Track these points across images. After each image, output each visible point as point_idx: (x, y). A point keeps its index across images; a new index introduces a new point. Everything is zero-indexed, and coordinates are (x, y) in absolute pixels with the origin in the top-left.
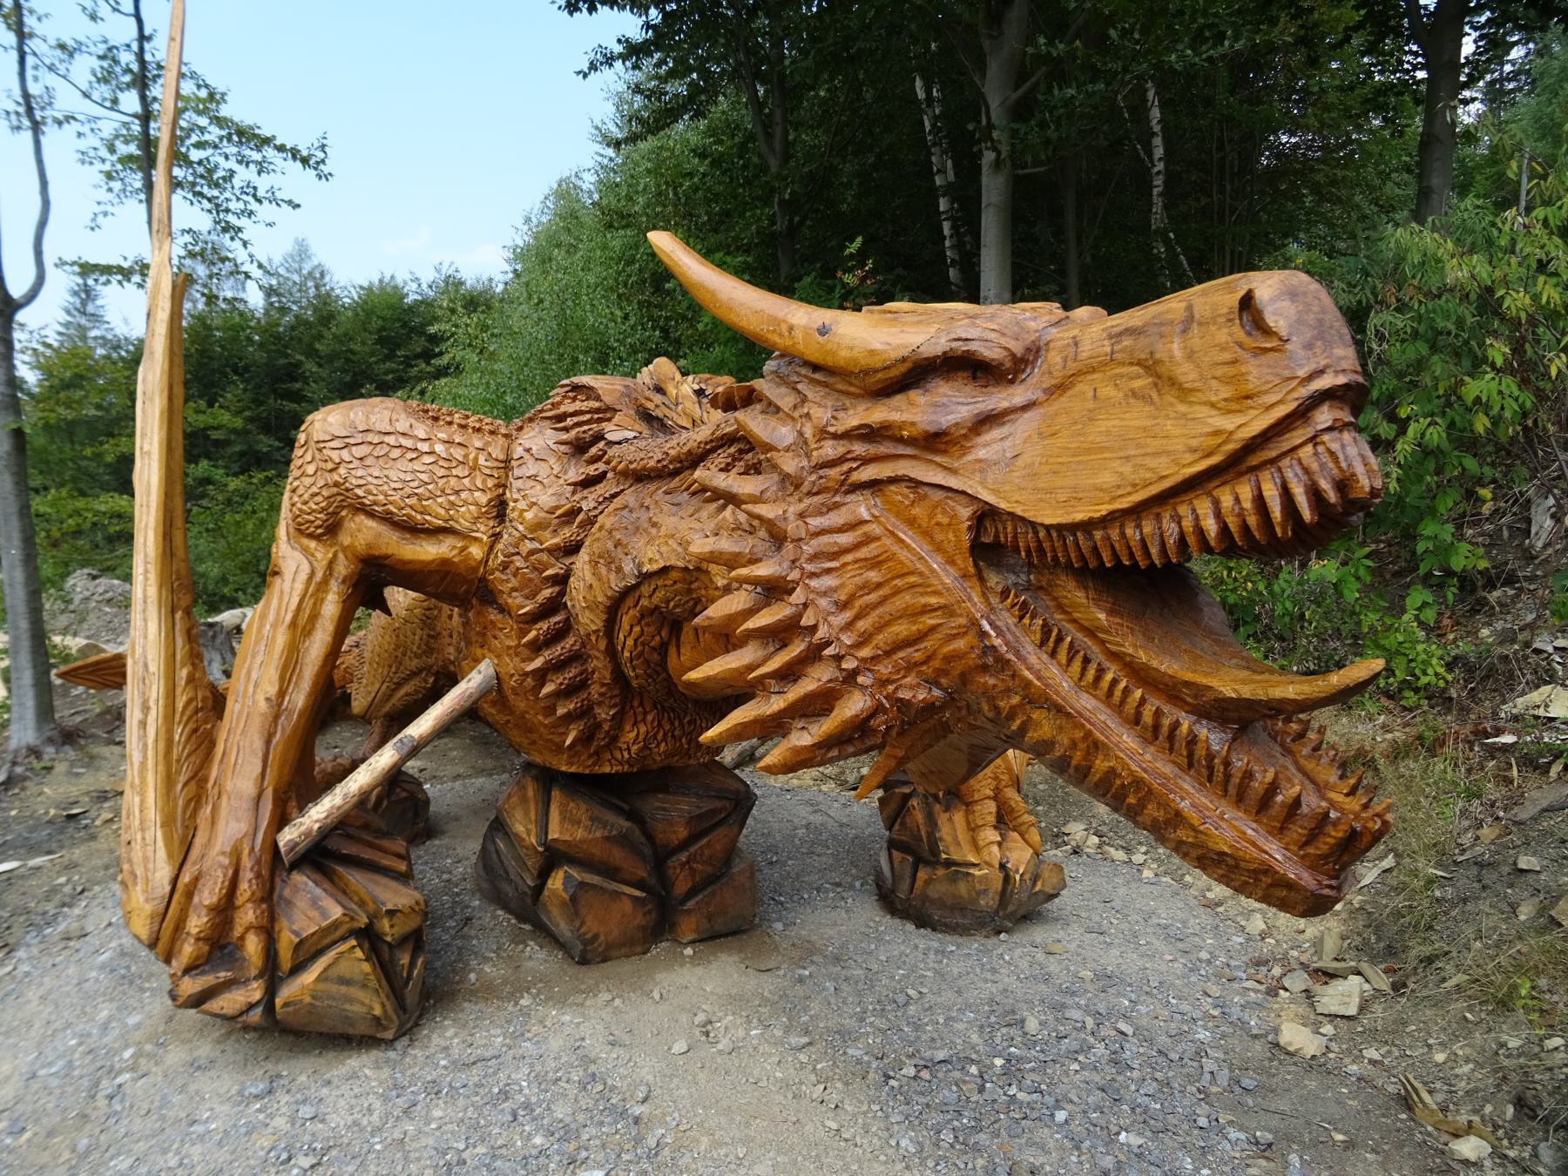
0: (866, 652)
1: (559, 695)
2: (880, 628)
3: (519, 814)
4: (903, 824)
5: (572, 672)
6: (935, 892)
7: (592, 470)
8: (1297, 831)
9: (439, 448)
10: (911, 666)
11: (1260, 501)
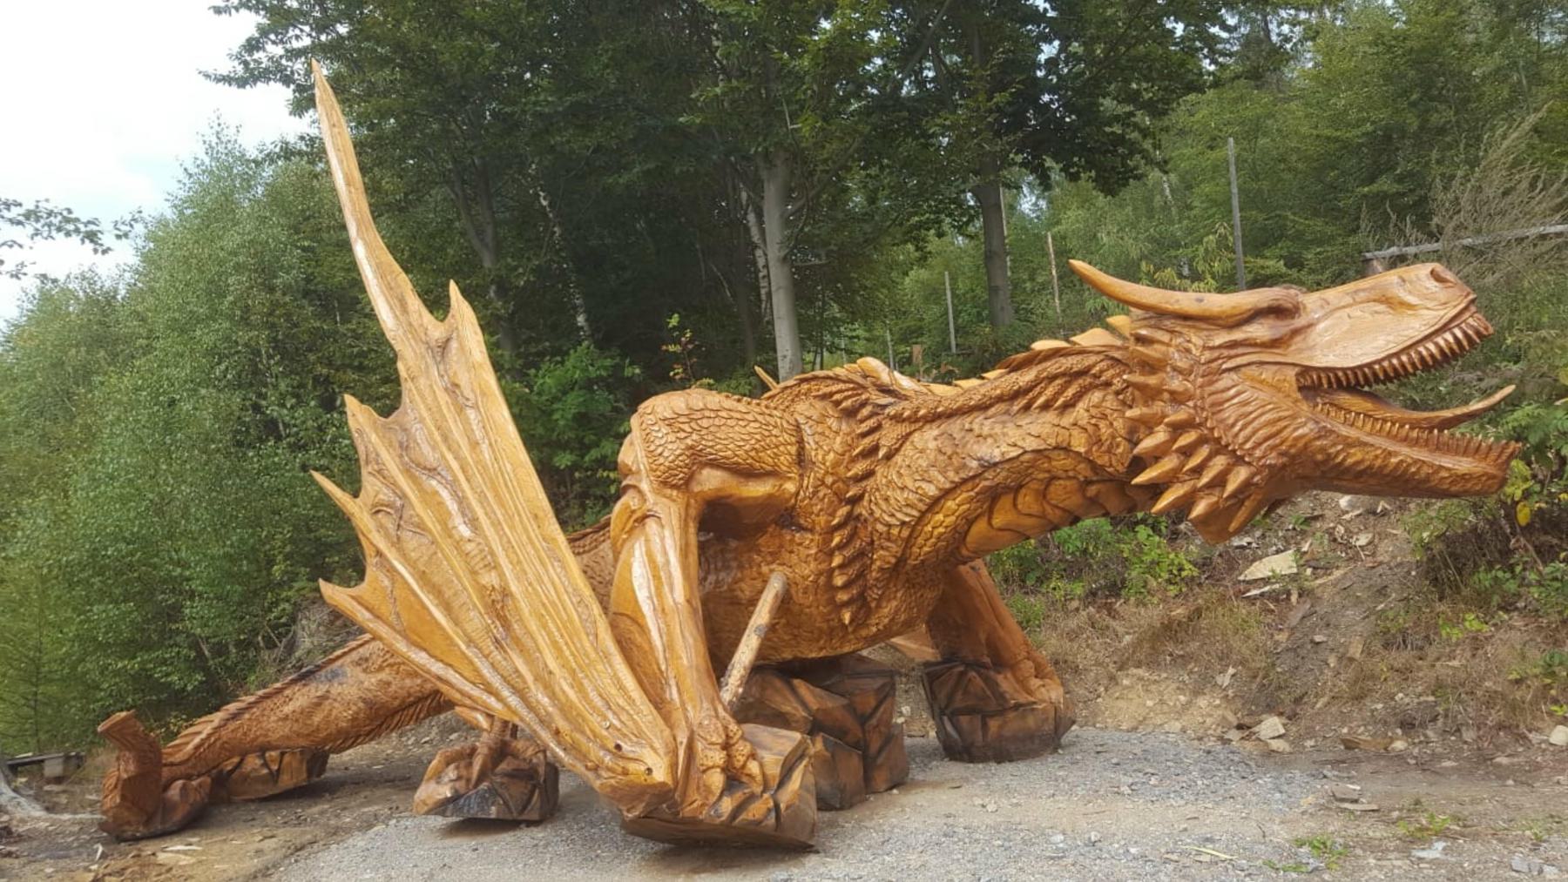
0: (1248, 446)
1: (846, 586)
2: (1254, 433)
3: (778, 699)
4: (966, 692)
5: (857, 566)
6: (1007, 732)
7: (871, 423)
8: (1493, 455)
9: (760, 418)
10: (1273, 448)
11: (1456, 338)
